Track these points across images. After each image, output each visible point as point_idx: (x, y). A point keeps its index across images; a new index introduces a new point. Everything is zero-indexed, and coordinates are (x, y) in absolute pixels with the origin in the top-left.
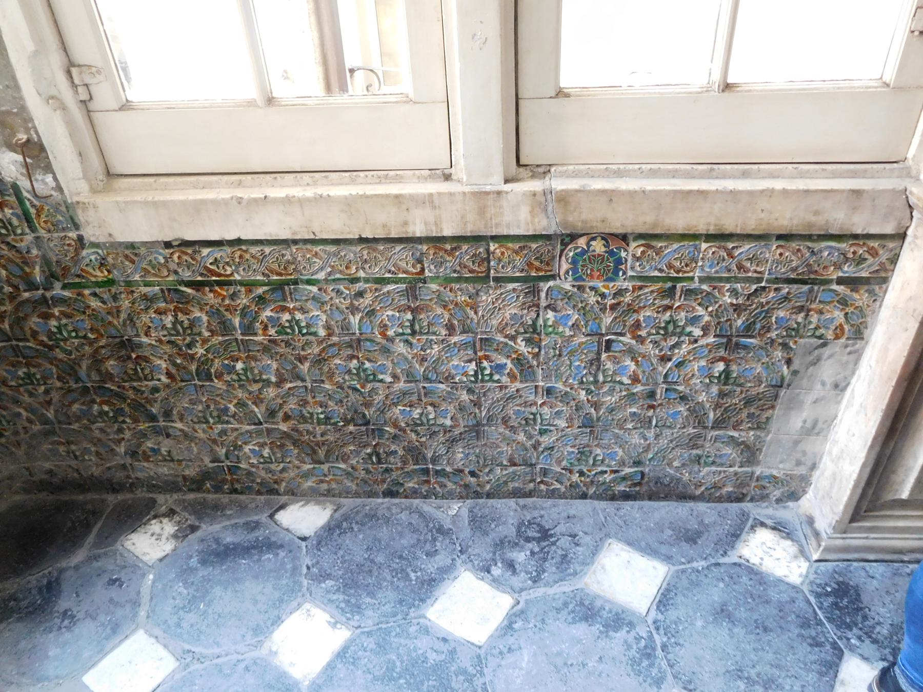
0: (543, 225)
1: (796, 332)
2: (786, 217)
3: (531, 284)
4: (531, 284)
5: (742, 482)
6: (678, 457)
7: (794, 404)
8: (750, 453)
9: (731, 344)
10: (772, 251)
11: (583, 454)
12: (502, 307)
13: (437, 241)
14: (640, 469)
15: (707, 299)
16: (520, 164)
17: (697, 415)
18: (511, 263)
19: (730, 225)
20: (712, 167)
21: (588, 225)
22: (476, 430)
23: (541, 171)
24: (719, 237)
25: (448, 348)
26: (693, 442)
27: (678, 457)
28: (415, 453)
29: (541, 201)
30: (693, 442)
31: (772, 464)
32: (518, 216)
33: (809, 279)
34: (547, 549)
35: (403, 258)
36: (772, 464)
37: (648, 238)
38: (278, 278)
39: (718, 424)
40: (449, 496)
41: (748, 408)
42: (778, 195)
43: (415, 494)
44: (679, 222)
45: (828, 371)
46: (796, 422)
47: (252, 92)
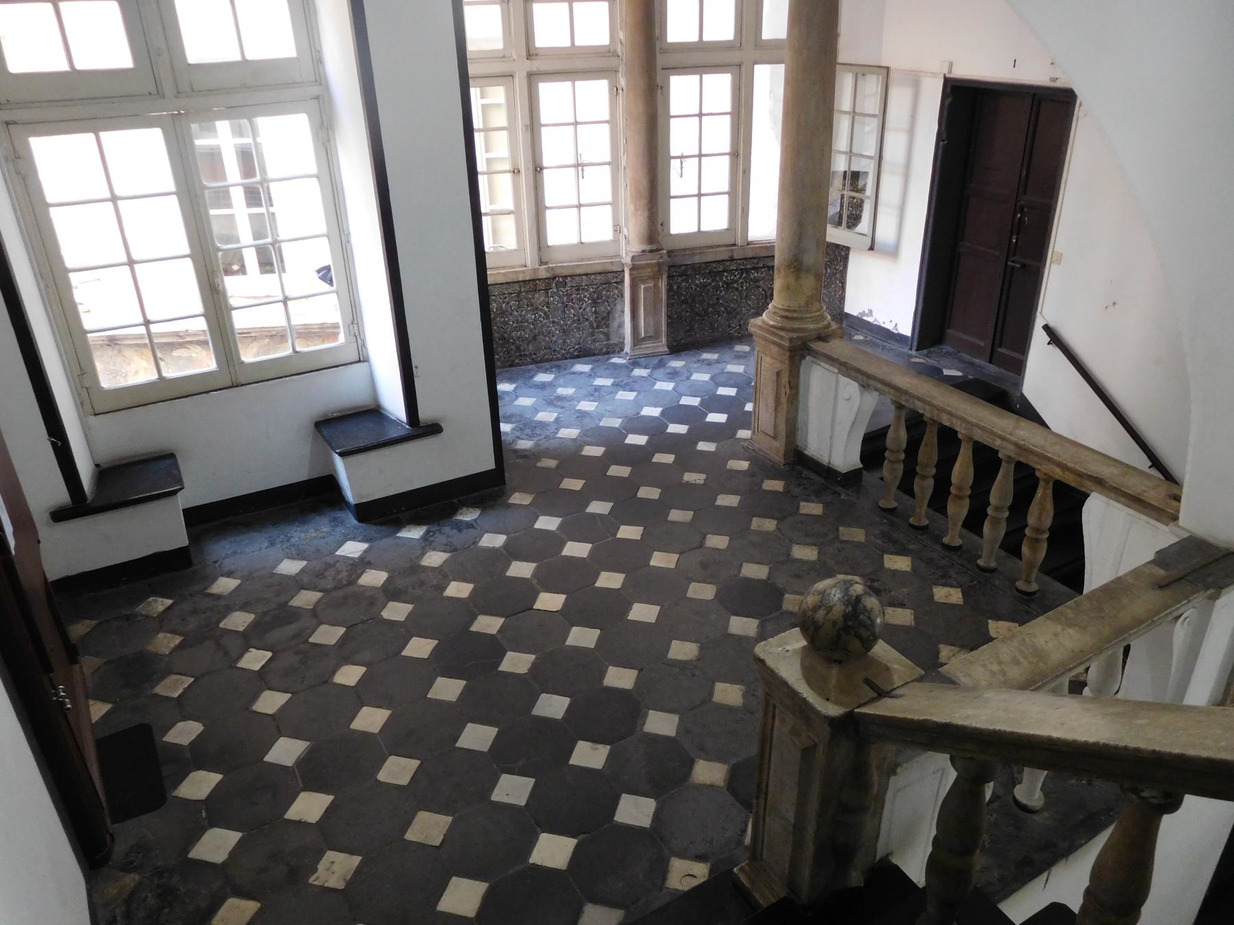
2: (599, 269)
7: (614, 318)
8: (607, 336)
9: (595, 303)
10: (599, 277)
11: (564, 342)
12: (540, 298)
13: (524, 281)
14: (931, 362)
15: (587, 290)
16: (542, 263)
18: (541, 286)
20: (582, 260)
21: (925, 351)
22: (535, 338)
23: (546, 263)
24: (587, 275)
25: (527, 311)
26: (592, 334)
28: (518, 348)
31: (614, 340)
32: (543, 274)
33: (609, 283)
35: (516, 287)
36: (614, 340)
37: (571, 276)
38: (976, 361)
39: (598, 327)
41: (604, 320)
43: (518, 365)
44: (578, 272)
45: (619, 307)
46: (616, 324)
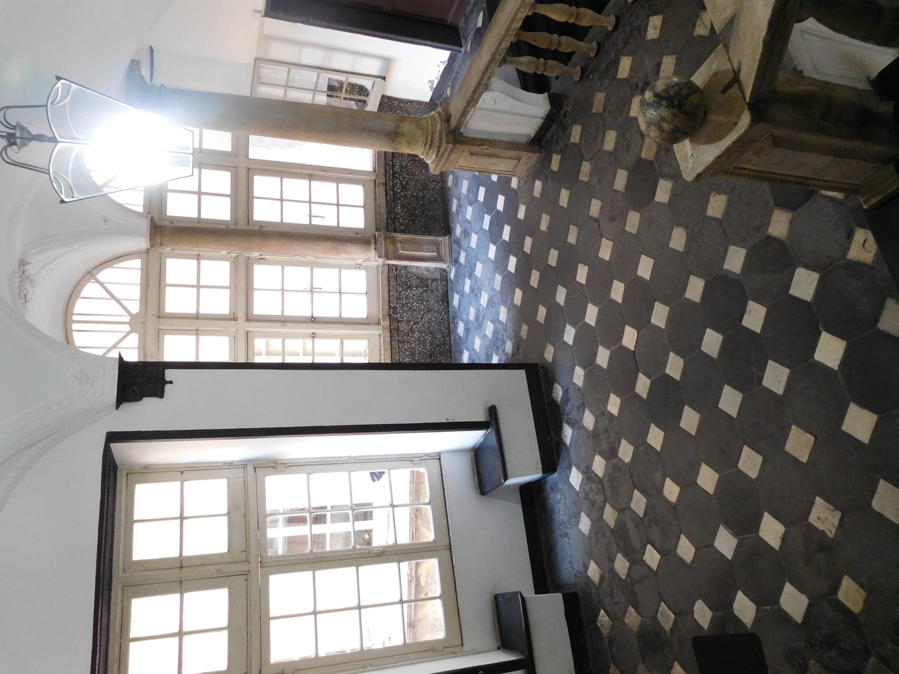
0: (388, 319)
1: (406, 277)
2: (386, 282)
3: (398, 322)
4: (398, 322)
5: (442, 281)
6: (436, 293)
9: (409, 287)
11: (436, 312)
12: (403, 327)
16: (379, 323)
17: (425, 291)
18: (395, 325)
19: (387, 290)
22: (431, 333)
23: (379, 320)
24: (389, 292)
26: (432, 291)
27: (436, 293)
28: (438, 346)
29: (384, 319)
30: (432, 291)
32: (387, 323)
34: (538, 58)
40: (450, 339)
41: (423, 282)
42: (382, 283)
44: (386, 298)
45: (414, 270)
46: (426, 273)
47: (203, 262)
